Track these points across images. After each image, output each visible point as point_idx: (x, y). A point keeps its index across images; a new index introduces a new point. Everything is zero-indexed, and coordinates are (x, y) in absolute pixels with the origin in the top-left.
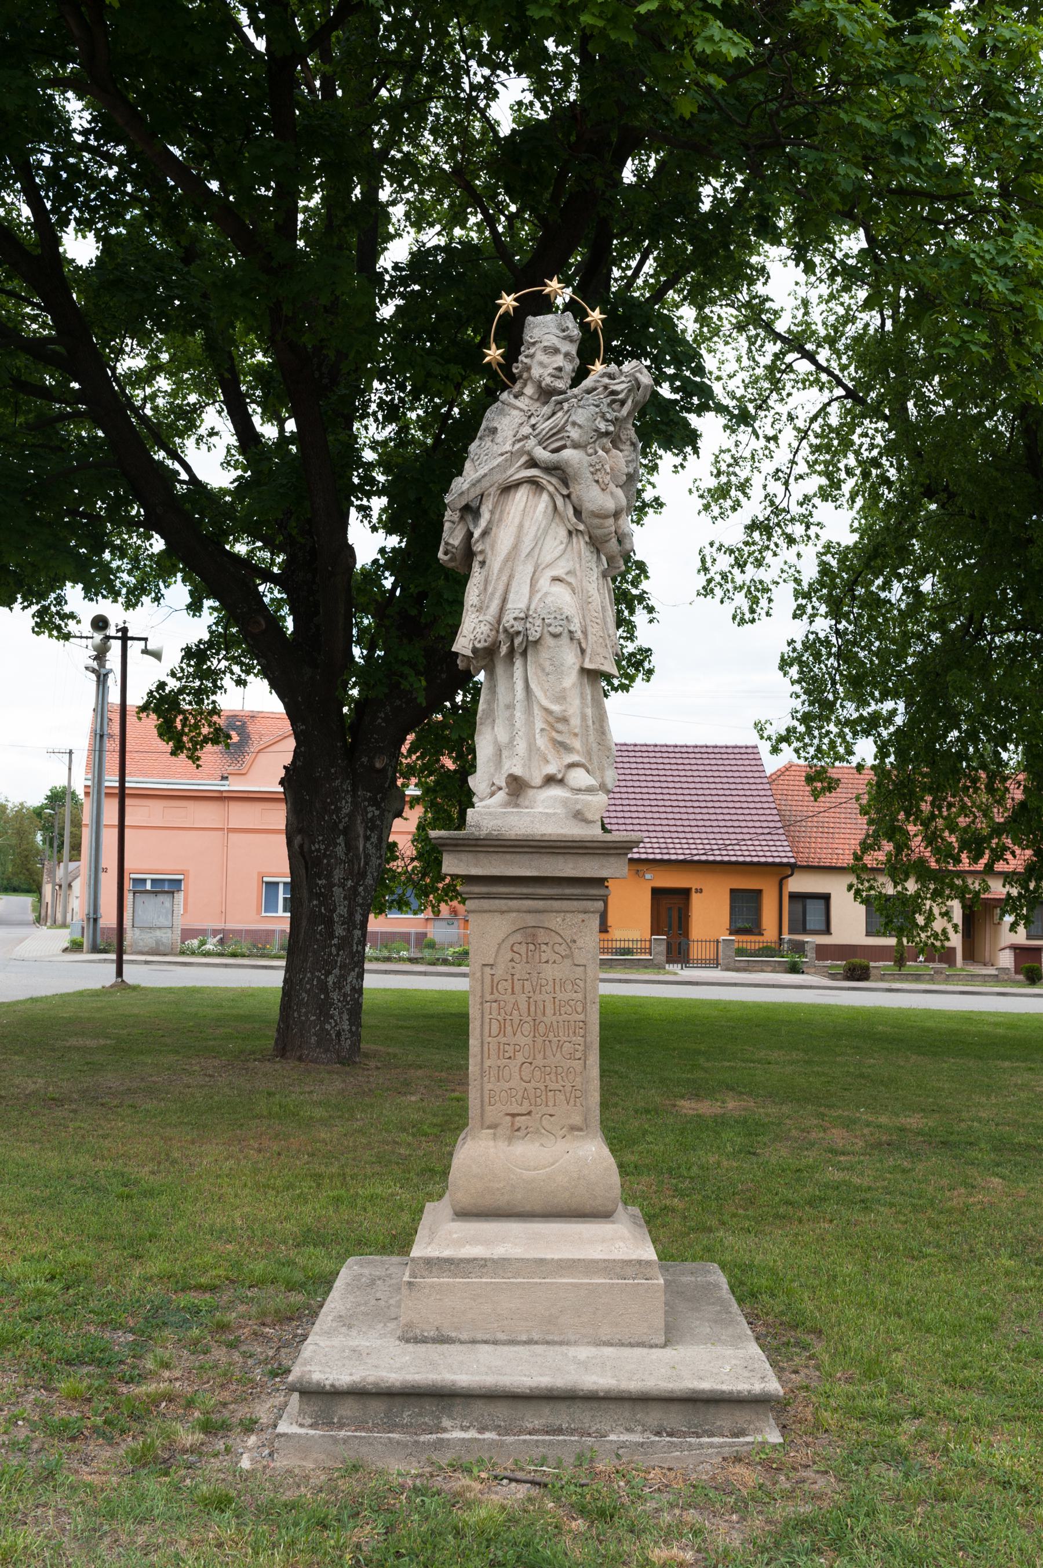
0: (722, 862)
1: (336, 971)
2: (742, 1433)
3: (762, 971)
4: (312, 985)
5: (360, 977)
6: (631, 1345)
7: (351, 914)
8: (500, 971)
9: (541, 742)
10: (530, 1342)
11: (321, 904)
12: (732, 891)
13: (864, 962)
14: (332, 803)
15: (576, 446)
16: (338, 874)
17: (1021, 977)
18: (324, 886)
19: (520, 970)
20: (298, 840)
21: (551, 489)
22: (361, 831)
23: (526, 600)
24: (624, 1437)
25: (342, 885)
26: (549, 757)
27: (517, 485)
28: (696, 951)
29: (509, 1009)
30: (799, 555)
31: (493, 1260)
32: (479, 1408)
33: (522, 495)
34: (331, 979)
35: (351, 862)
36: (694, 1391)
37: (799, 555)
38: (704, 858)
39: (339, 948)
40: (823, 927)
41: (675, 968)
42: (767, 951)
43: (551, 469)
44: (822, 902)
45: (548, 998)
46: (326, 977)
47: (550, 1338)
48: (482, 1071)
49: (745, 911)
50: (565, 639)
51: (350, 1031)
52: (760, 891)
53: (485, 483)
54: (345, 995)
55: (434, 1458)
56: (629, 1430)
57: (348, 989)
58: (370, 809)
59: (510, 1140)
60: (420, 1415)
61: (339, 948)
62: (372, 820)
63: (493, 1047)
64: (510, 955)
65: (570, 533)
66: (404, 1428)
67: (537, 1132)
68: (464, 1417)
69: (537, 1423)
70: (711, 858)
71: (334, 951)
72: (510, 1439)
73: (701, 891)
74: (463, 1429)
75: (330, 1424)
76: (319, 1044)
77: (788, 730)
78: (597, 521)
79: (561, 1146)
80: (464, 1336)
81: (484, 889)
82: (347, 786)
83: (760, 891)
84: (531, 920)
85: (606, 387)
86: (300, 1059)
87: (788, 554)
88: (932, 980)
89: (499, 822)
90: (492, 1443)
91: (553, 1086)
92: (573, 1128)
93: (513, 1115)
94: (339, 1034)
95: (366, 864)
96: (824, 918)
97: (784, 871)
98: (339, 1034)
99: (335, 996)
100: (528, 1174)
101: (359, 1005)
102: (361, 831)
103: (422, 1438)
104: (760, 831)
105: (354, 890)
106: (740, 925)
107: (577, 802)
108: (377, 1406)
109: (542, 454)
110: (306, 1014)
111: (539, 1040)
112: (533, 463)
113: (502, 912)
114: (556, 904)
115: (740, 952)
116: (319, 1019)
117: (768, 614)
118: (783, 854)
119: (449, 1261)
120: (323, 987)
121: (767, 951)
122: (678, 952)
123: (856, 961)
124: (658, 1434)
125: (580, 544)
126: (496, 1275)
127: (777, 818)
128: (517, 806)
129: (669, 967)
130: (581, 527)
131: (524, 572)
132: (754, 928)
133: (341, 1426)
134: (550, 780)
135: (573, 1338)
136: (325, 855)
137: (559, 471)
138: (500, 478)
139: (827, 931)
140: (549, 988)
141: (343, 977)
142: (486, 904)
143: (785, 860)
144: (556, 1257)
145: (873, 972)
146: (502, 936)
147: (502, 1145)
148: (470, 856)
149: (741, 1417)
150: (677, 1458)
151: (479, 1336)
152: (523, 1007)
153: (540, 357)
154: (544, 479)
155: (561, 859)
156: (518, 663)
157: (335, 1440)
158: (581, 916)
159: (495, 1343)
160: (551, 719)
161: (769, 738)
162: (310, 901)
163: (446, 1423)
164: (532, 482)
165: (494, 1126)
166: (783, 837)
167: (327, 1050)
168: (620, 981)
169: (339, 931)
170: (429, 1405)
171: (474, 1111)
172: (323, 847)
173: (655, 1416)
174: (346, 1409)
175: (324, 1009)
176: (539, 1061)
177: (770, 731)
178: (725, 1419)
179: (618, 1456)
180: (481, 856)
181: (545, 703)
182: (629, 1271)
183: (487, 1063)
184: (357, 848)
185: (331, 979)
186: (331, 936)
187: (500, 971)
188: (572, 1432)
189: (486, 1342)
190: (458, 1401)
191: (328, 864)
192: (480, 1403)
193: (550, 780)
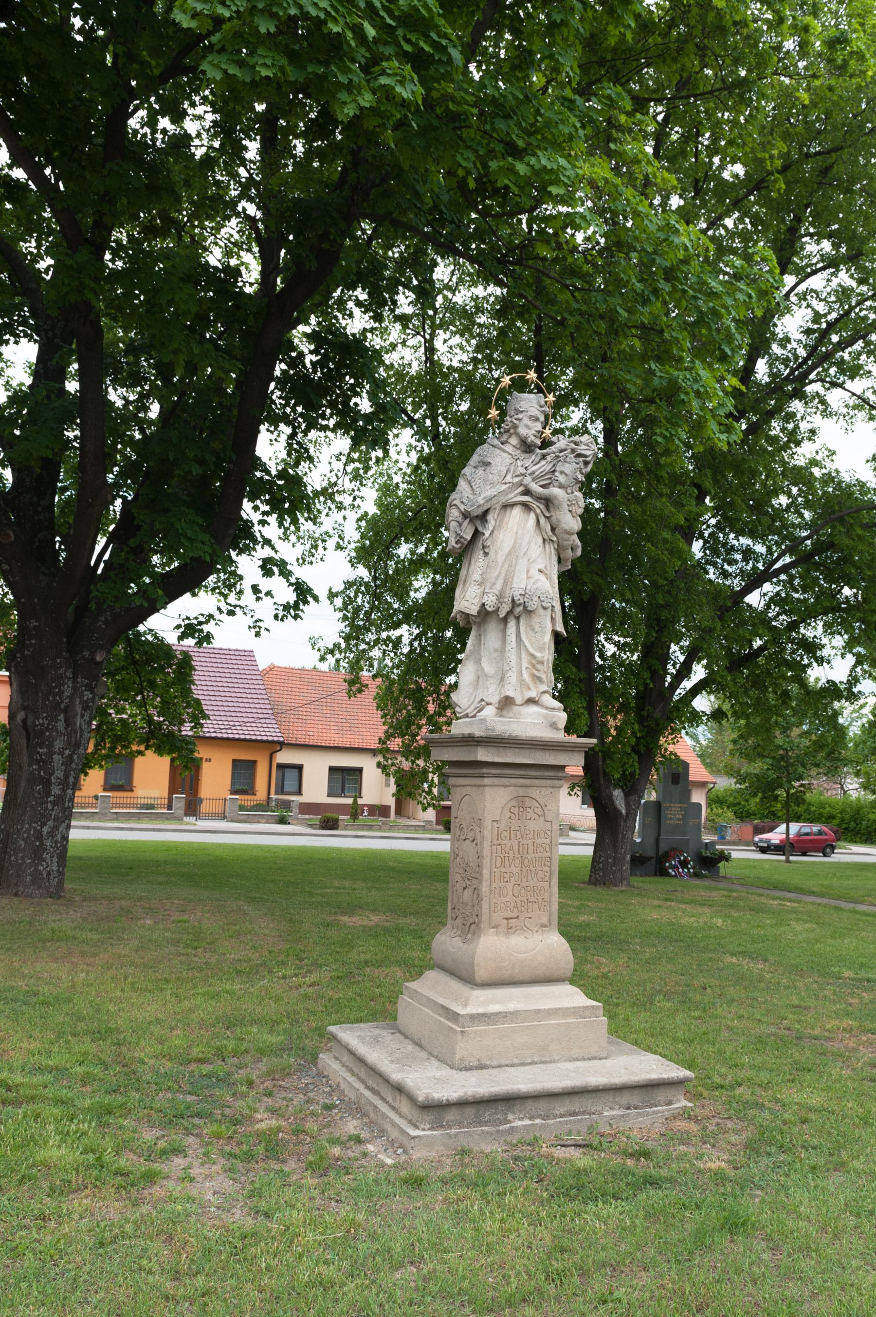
0: (228, 739)
1: (51, 823)
2: (669, 1103)
3: (259, 822)
4: (29, 834)
5: (69, 827)
6: (589, 1059)
7: (67, 777)
8: (502, 825)
9: (526, 676)
10: (533, 1063)
11: (40, 768)
12: (234, 761)
13: (334, 815)
14: (56, 687)
15: (561, 486)
16: (58, 745)
17: (441, 827)
18: (45, 754)
19: (515, 824)
20: (21, 715)
21: (538, 511)
22: (79, 711)
23: (524, 582)
24: (613, 1113)
25: (61, 754)
26: (531, 686)
27: (513, 505)
28: (204, 808)
29: (507, 850)
30: (345, 518)
31: (510, 1013)
32: (530, 1105)
33: (517, 511)
34: (45, 829)
35: (69, 735)
36: (650, 1080)
37: (345, 518)
38: (213, 735)
39: (54, 804)
40: (296, 789)
41: (192, 819)
42: (258, 807)
43: (539, 498)
44: (296, 771)
45: (530, 842)
46: (42, 827)
47: (544, 1059)
48: (491, 891)
49: (243, 776)
50: (549, 612)
51: (58, 871)
52: (255, 762)
53: (494, 501)
54: (56, 842)
55: (509, 1140)
56: (612, 1109)
57: (59, 837)
58: (86, 693)
59: (507, 934)
60: (496, 1114)
61: (54, 804)
62: (87, 702)
63: (498, 874)
64: (509, 814)
65: (544, 540)
66: (486, 1123)
67: (522, 929)
68: (520, 1112)
69: (562, 1111)
70: (219, 735)
71: (50, 806)
72: (551, 1122)
73: (210, 760)
74: (520, 1119)
75: (442, 1126)
76: (33, 882)
77: (335, 645)
78: (567, 536)
79: (537, 937)
80: (494, 1063)
81: (498, 771)
82: (69, 674)
83: (255, 762)
84: (522, 792)
85: (573, 451)
86: (16, 895)
87: (337, 516)
88: (380, 829)
89: (506, 728)
90: (542, 1126)
91: (531, 899)
92: (543, 926)
93: (507, 919)
94: (49, 874)
95: (81, 736)
96: (297, 783)
97: (274, 746)
98: (49, 874)
99: (48, 843)
100: (521, 956)
101: (65, 848)
102: (79, 711)
103: (501, 1128)
104: (261, 716)
105: (71, 757)
106: (238, 787)
107: (554, 716)
108: (470, 1111)
109: (535, 487)
110: (23, 858)
111: (524, 869)
112: (527, 492)
113: (505, 786)
114: (537, 782)
115: (242, 808)
116: (33, 861)
117: (322, 559)
118: (272, 734)
119: (484, 1015)
120: (39, 836)
121: (258, 807)
122: (193, 808)
123: (330, 815)
124: (628, 1108)
125: (551, 549)
126: (512, 1022)
127: (269, 707)
128: (501, 716)
129: (187, 819)
130: (554, 539)
131: (522, 565)
132: (249, 790)
133: (450, 1127)
134: (531, 701)
135: (557, 1058)
136: (48, 729)
137: (548, 502)
138: (503, 500)
139: (299, 792)
140: (531, 836)
141: (56, 828)
142: (497, 781)
143: (276, 739)
144: (547, 1007)
145: (341, 823)
146: (504, 802)
147: (502, 938)
148: (494, 749)
149: (669, 1093)
150: (641, 1122)
151: (503, 1062)
152: (516, 848)
153: (526, 421)
154: (534, 504)
155: (445, 750)
156: (512, 624)
157: (449, 1136)
158: (551, 790)
159: (513, 1065)
160: (534, 661)
161: (319, 650)
162: (30, 765)
163: (510, 1117)
164: (526, 506)
165: (496, 927)
166: (273, 721)
167: (39, 887)
168: (154, 830)
169: (55, 790)
170: (501, 1107)
171: (485, 918)
172: (46, 722)
173: (626, 1098)
174: (451, 1116)
175: (38, 854)
176: (524, 884)
177: (321, 644)
178: (661, 1095)
179: (610, 1125)
180: (501, 749)
181: (532, 651)
182: (587, 1013)
183: (494, 885)
184: (75, 724)
185: (45, 829)
186: (48, 794)
187: (502, 825)
188: (584, 1113)
189: (507, 1066)
190: (518, 1102)
191: (50, 736)
192: (530, 1102)
193: (531, 701)
